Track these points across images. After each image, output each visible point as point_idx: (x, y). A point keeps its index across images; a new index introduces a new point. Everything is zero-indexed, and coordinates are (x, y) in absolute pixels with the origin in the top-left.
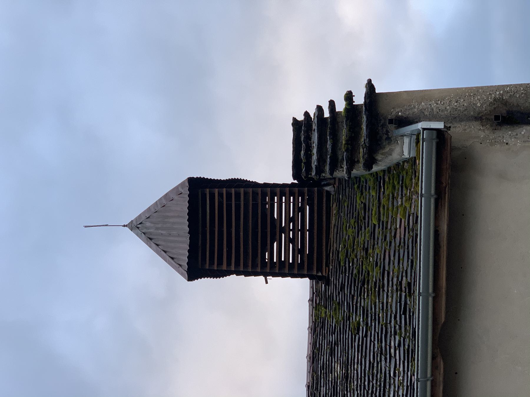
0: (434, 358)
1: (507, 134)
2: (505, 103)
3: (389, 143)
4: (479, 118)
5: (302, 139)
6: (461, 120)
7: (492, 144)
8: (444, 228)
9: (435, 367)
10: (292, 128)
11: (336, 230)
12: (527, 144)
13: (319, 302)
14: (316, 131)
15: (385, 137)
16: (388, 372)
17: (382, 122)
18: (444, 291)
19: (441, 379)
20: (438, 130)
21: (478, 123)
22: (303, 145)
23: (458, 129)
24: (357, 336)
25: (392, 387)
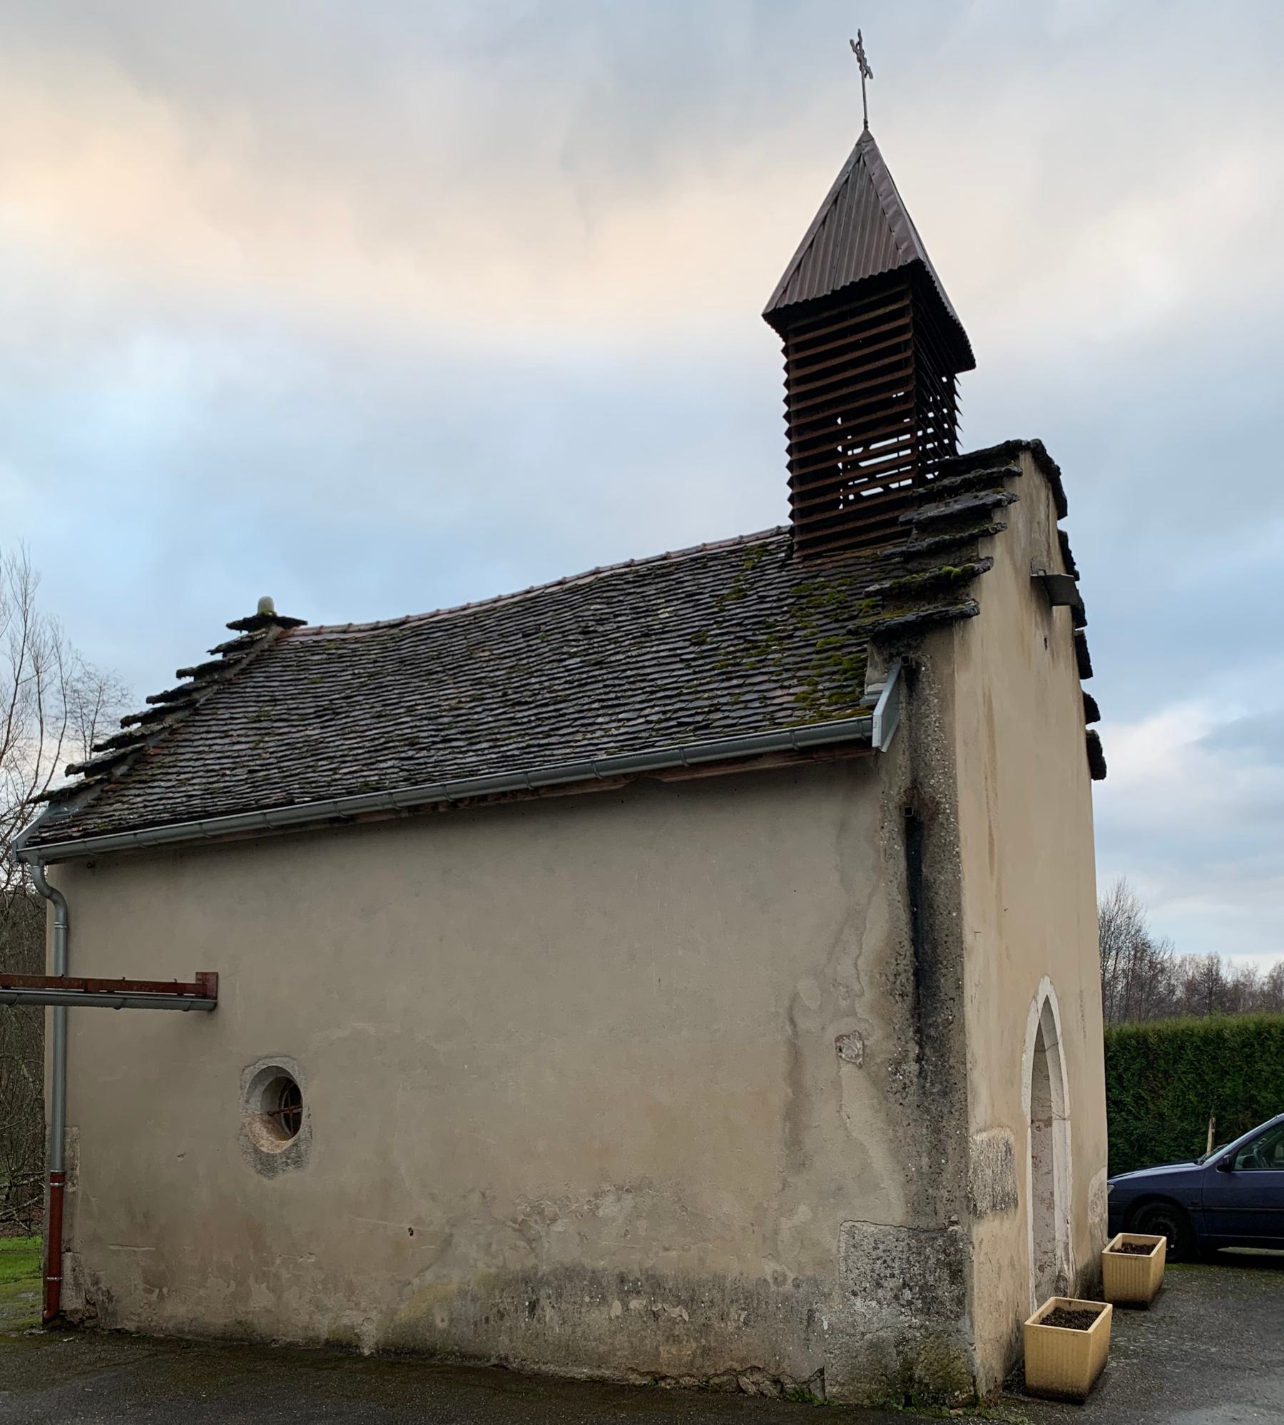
0: (625, 776)
1: (894, 825)
2: (933, 819)
3: (885, 660)
4: (915, 785)
5: (967, 476)
6: (912, 760)
7: (882, 807)
8: (766, 765)
9: (615, 779)
10: (1002, 442)
11: (850, 562)
12: (882, 854)
13: (744, 555)
14: (978, 502)
15: (894, 651)
16: (626, 708)
17: (914, 644)
18: (696, 776)
19: (605, 788)
20: (870, 738)
21: (909, 785)
22: (959, 479)
23: (901, 757)
24: (687, 643)
25: (607, 719)
